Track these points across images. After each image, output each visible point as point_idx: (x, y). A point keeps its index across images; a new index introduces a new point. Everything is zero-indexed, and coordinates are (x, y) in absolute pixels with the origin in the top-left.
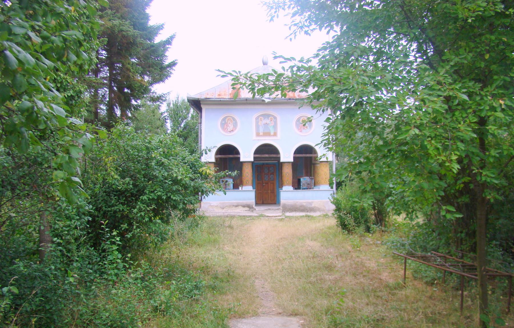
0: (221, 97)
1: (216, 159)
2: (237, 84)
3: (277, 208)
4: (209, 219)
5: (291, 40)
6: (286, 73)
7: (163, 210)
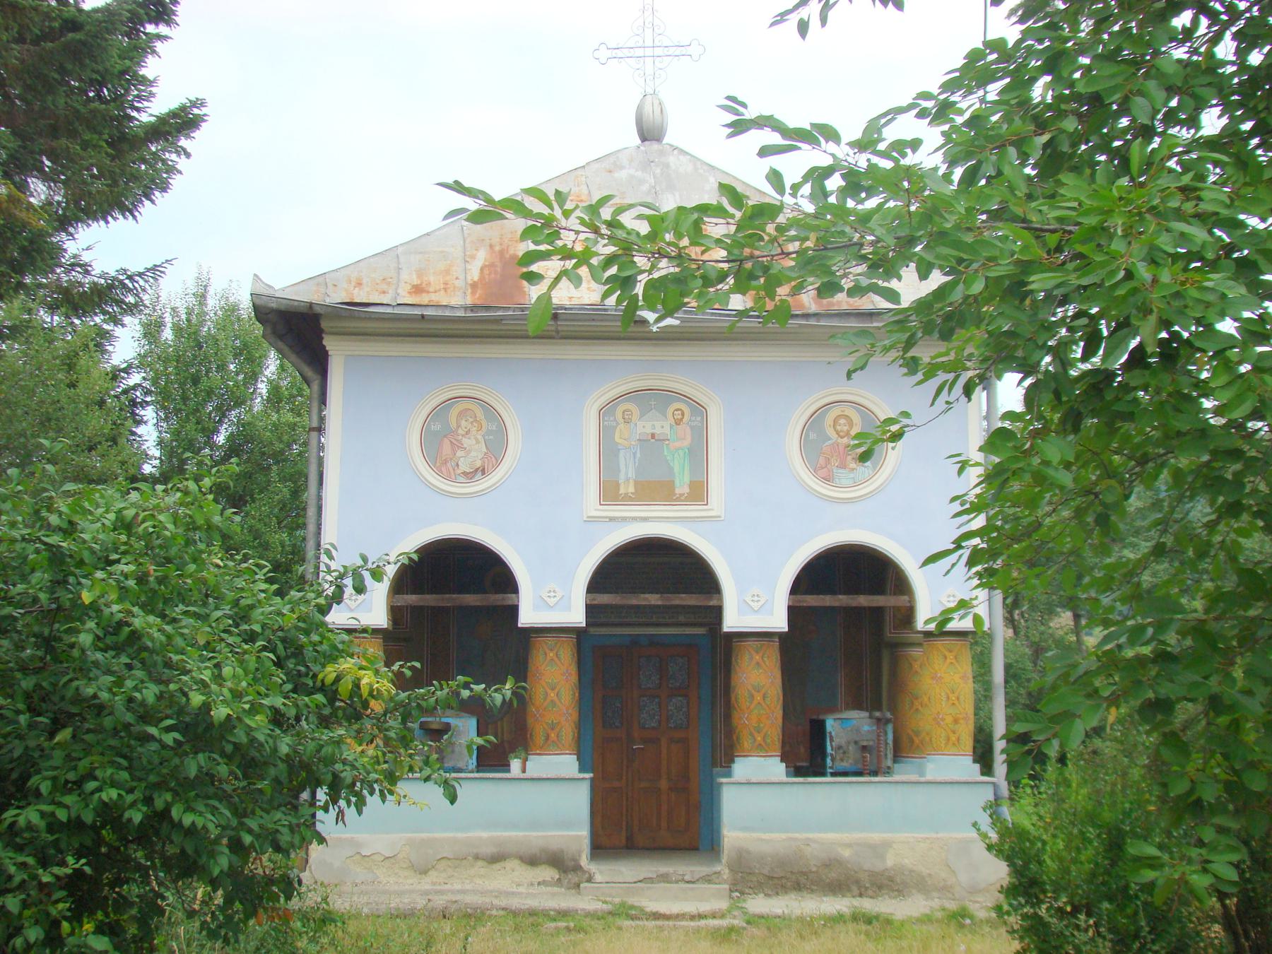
0: (424, 299)
2: (544, 256)
3: (700, 869)
4: (352, 927)
5: (803, 28)
6: (788, 199)
7: (118, 882)
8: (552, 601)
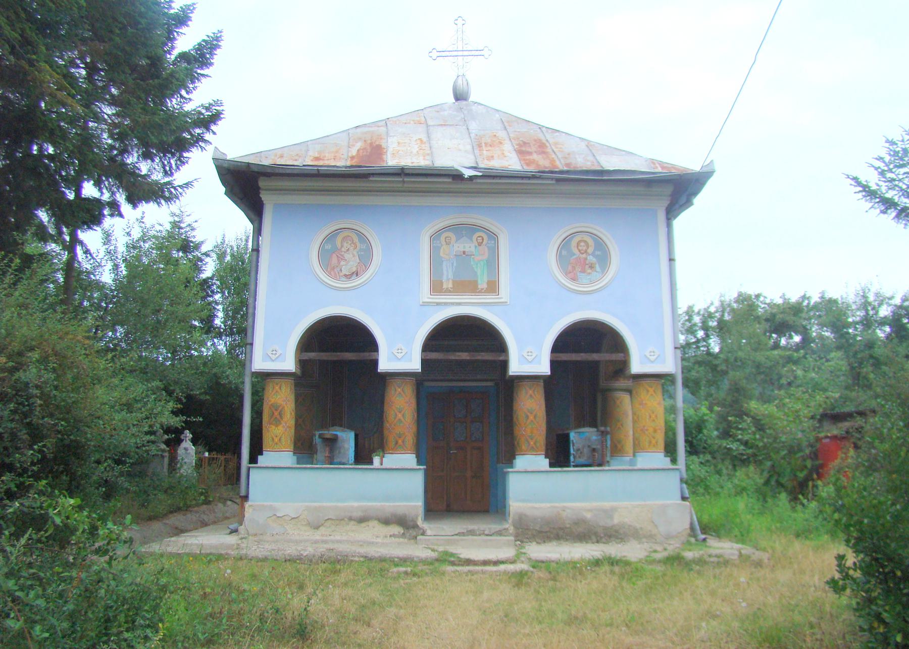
0: (321, 163)
1: (302, 363)
3: (495, 527)
8: (399, 356)
